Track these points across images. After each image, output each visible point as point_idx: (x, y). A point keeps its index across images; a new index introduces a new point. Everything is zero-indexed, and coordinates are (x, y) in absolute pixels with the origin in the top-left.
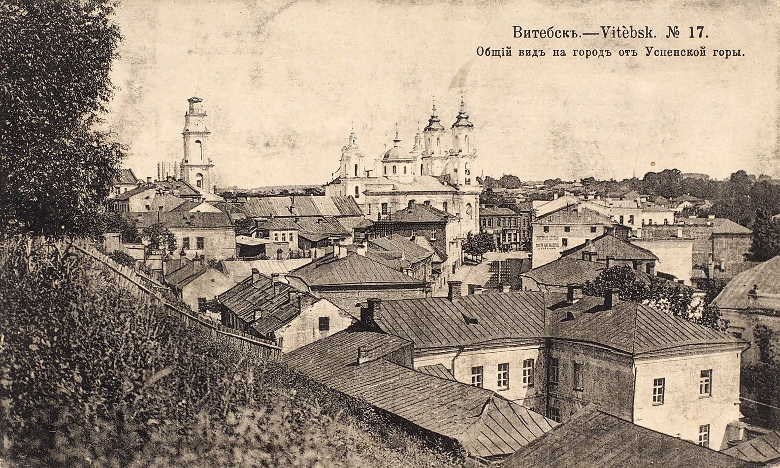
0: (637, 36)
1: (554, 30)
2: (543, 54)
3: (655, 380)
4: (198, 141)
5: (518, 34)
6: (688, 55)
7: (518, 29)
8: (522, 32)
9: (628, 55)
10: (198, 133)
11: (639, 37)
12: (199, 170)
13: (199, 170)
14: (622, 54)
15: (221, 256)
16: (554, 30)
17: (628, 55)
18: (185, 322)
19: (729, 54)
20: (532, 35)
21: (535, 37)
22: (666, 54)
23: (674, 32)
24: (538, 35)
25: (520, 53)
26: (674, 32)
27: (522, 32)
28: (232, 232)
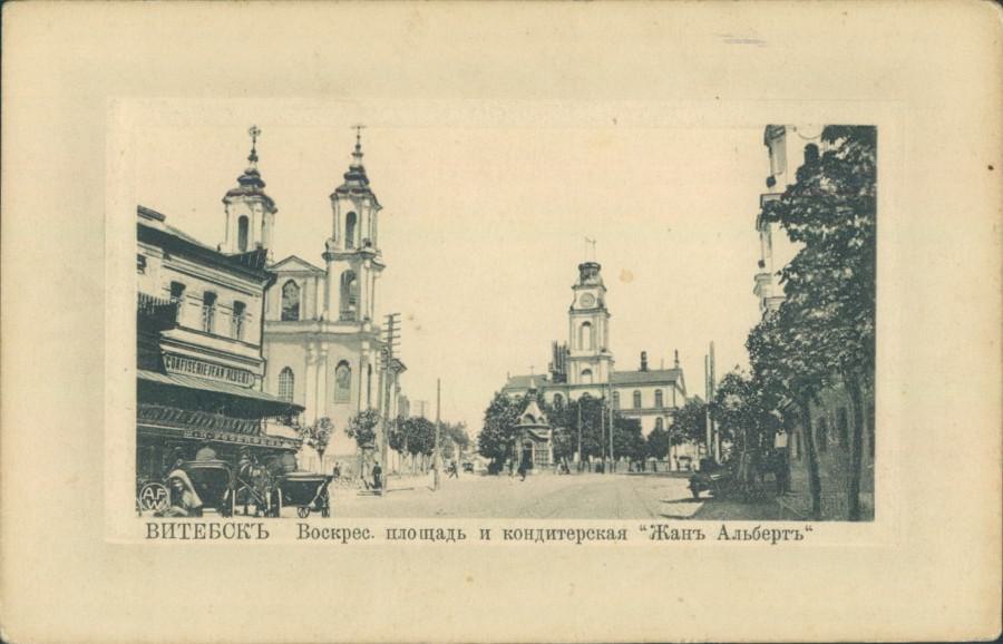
0: (222, 527)
1: (761, 530)
2: (462, 536)
3: (859, 511)
4: (587, 324)
5: (153, 534)
9: (786, 539)
10: (585, 359)
11: (218, 525)
12: (585, 366)
13: (585, 366)
14: (412, 532)
15: (365, 235)
16: (761, 530)
17: (786, 539)
18: (712, 419)
19: (777, 537)
20: (557, 535)
21: (561, 538)
22: (418, 533)
23: (486, 534)
24: (564, 535)
26: (486, 534)
28: (275, 256)
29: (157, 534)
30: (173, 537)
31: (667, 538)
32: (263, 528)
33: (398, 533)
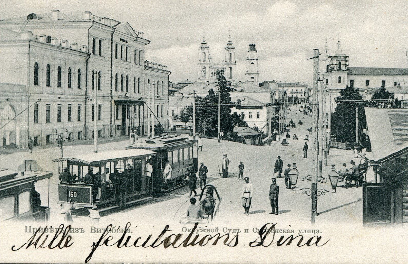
2: (82, 231)
5: (93, 231)
6: (284, 233)
7: (93, 228)
8: (96, 230)
25: (293, 231)
27: (96, 230)
29: (95, 231)
30: (308, 230)
31: (285, 232)
32: (83, 230)
33: (307, 231)
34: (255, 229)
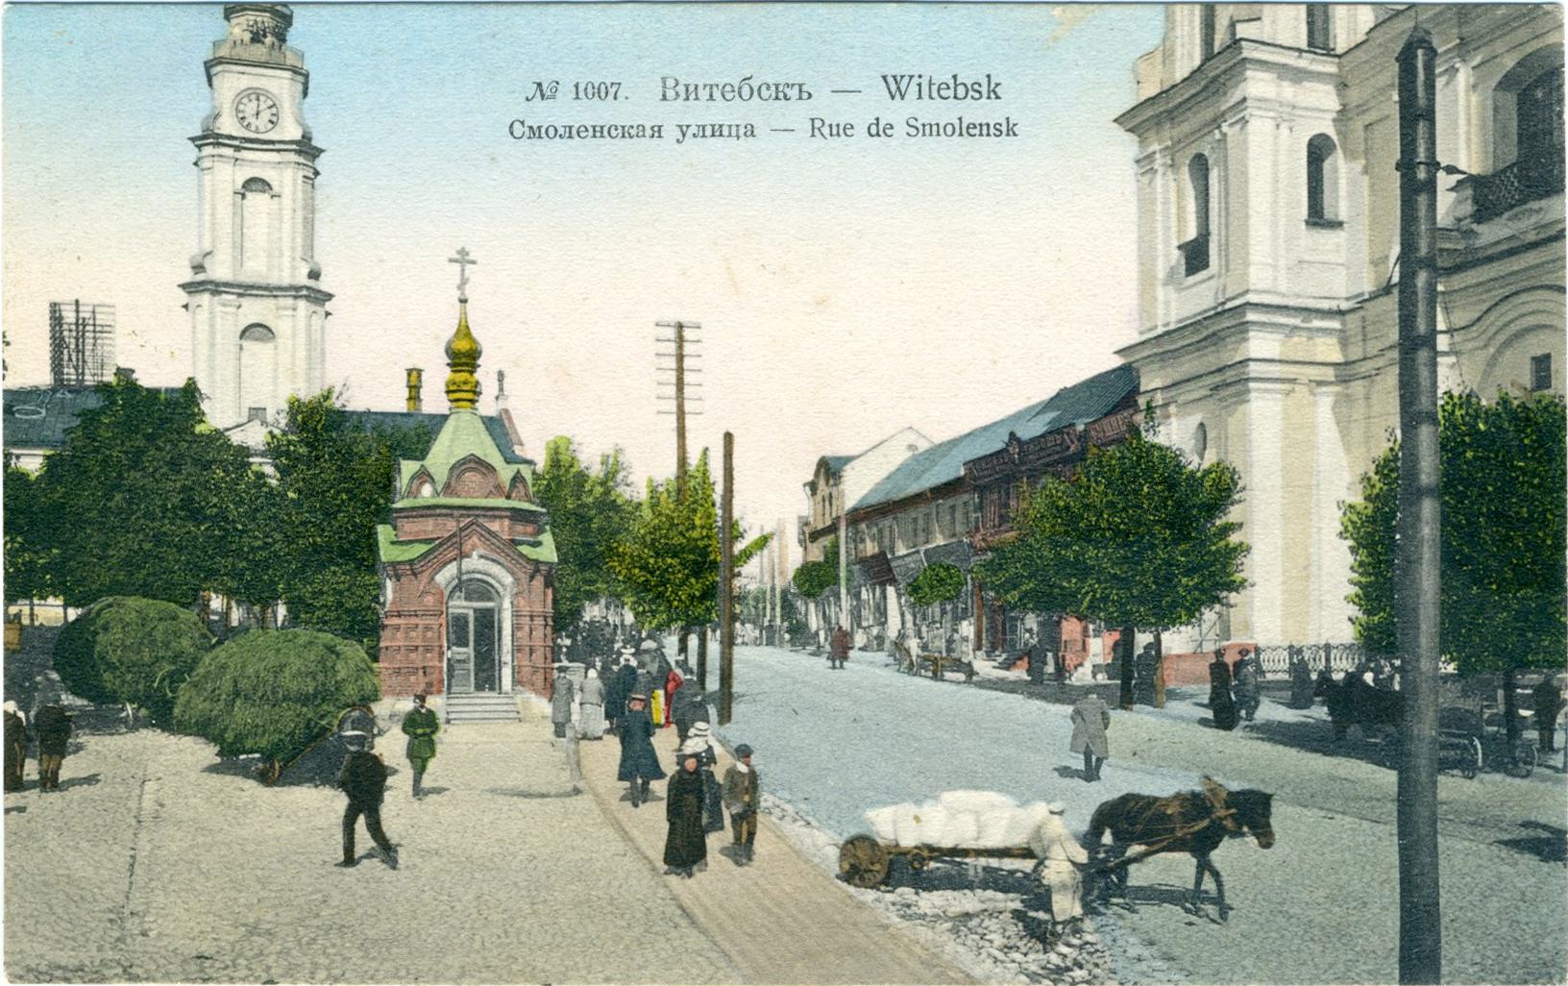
5: (671, 94)
8: (681, 89)
20: (704, 94)
24: (717, 94)
34: (518, 129)
